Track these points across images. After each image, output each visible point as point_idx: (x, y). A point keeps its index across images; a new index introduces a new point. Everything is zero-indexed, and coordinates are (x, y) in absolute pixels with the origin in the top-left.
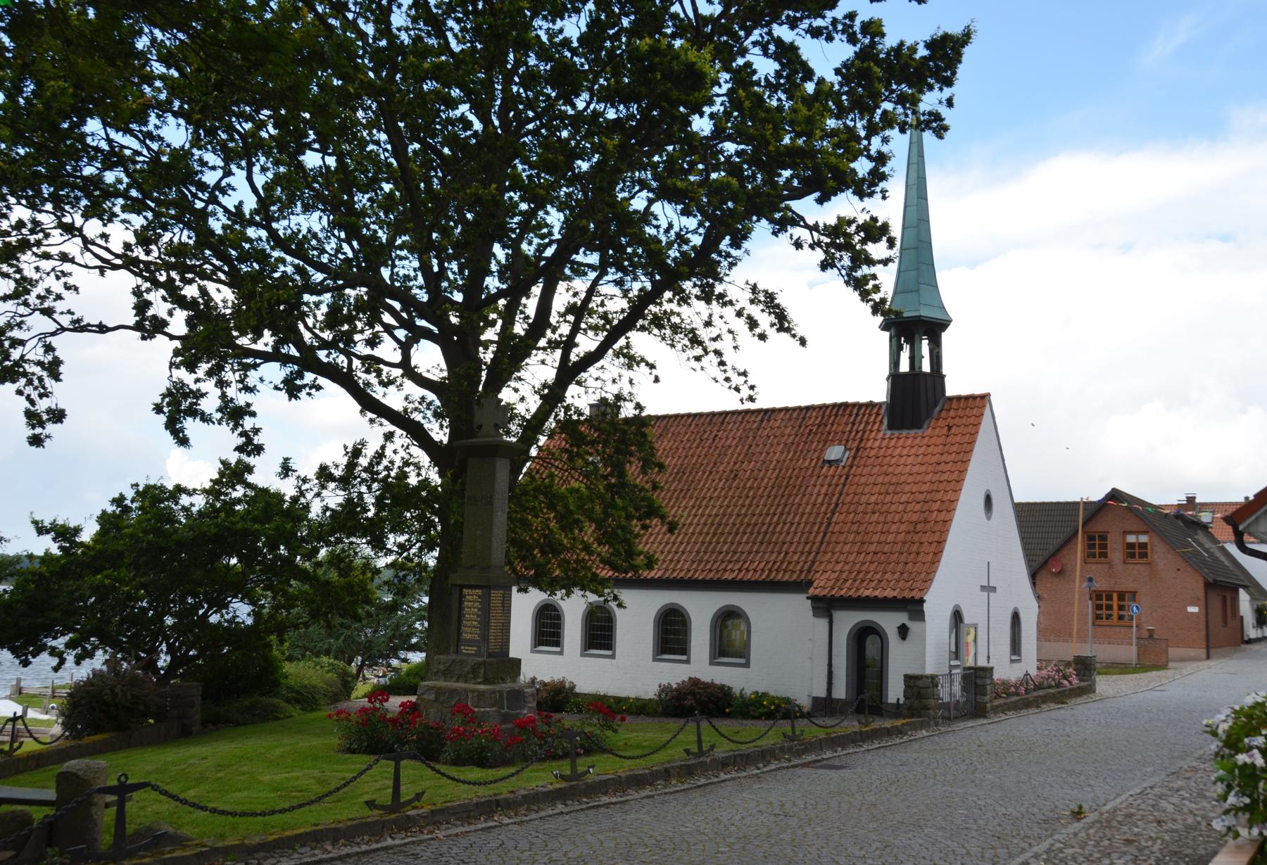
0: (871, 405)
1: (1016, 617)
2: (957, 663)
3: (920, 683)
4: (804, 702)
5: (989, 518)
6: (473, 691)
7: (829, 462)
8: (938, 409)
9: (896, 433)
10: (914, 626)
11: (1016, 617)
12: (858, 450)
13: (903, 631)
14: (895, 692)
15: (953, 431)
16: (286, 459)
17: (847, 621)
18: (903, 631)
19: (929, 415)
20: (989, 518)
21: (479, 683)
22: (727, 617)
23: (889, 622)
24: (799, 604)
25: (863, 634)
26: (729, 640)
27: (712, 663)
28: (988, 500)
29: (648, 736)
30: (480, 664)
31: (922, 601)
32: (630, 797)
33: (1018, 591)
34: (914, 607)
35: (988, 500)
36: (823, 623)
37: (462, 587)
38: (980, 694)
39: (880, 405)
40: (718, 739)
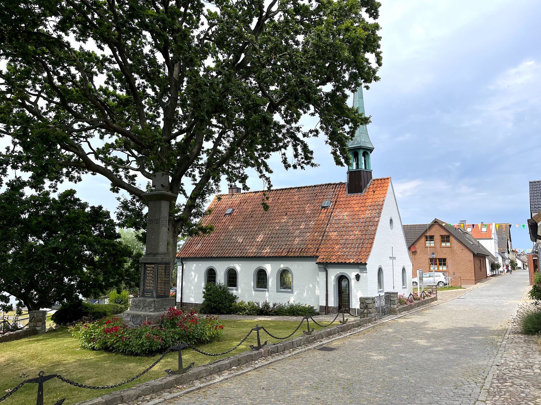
0: (341, 184)
1: (404, 270)
2: (381, 290)
3: (367, 301)
4: (317, 308)
5: (392, 229)
6: (148, 316)
7: (324, 207)
8: (369, 184)
9: (352, 195)
10: (362, 275)
11: (404, 270)
12: (336, 202)
13: (358, 277)
14: (355, 304)
15: (375, 193)
16: (358, 280)
17: (334, 273)
18: (358, 277)
19: (365, 187)
20: (392, 229)
21: (151, 312)
22: (283, 273)
23: (352, 274)
24: (311, 265)
25: (341, 278)
26: (284, 283)
27: (278, 291)
28: (391, 220)
29: (256, 320)
30: (152, 302)
31: (366, 264)
32: (215, 381)
33: (404, 258)
34: (361, 265)
35: (391, 220)
36: (323, 275)
37: (145, 263)
38: (392, 304)
39: (345, 183)
40: (269, 338)
